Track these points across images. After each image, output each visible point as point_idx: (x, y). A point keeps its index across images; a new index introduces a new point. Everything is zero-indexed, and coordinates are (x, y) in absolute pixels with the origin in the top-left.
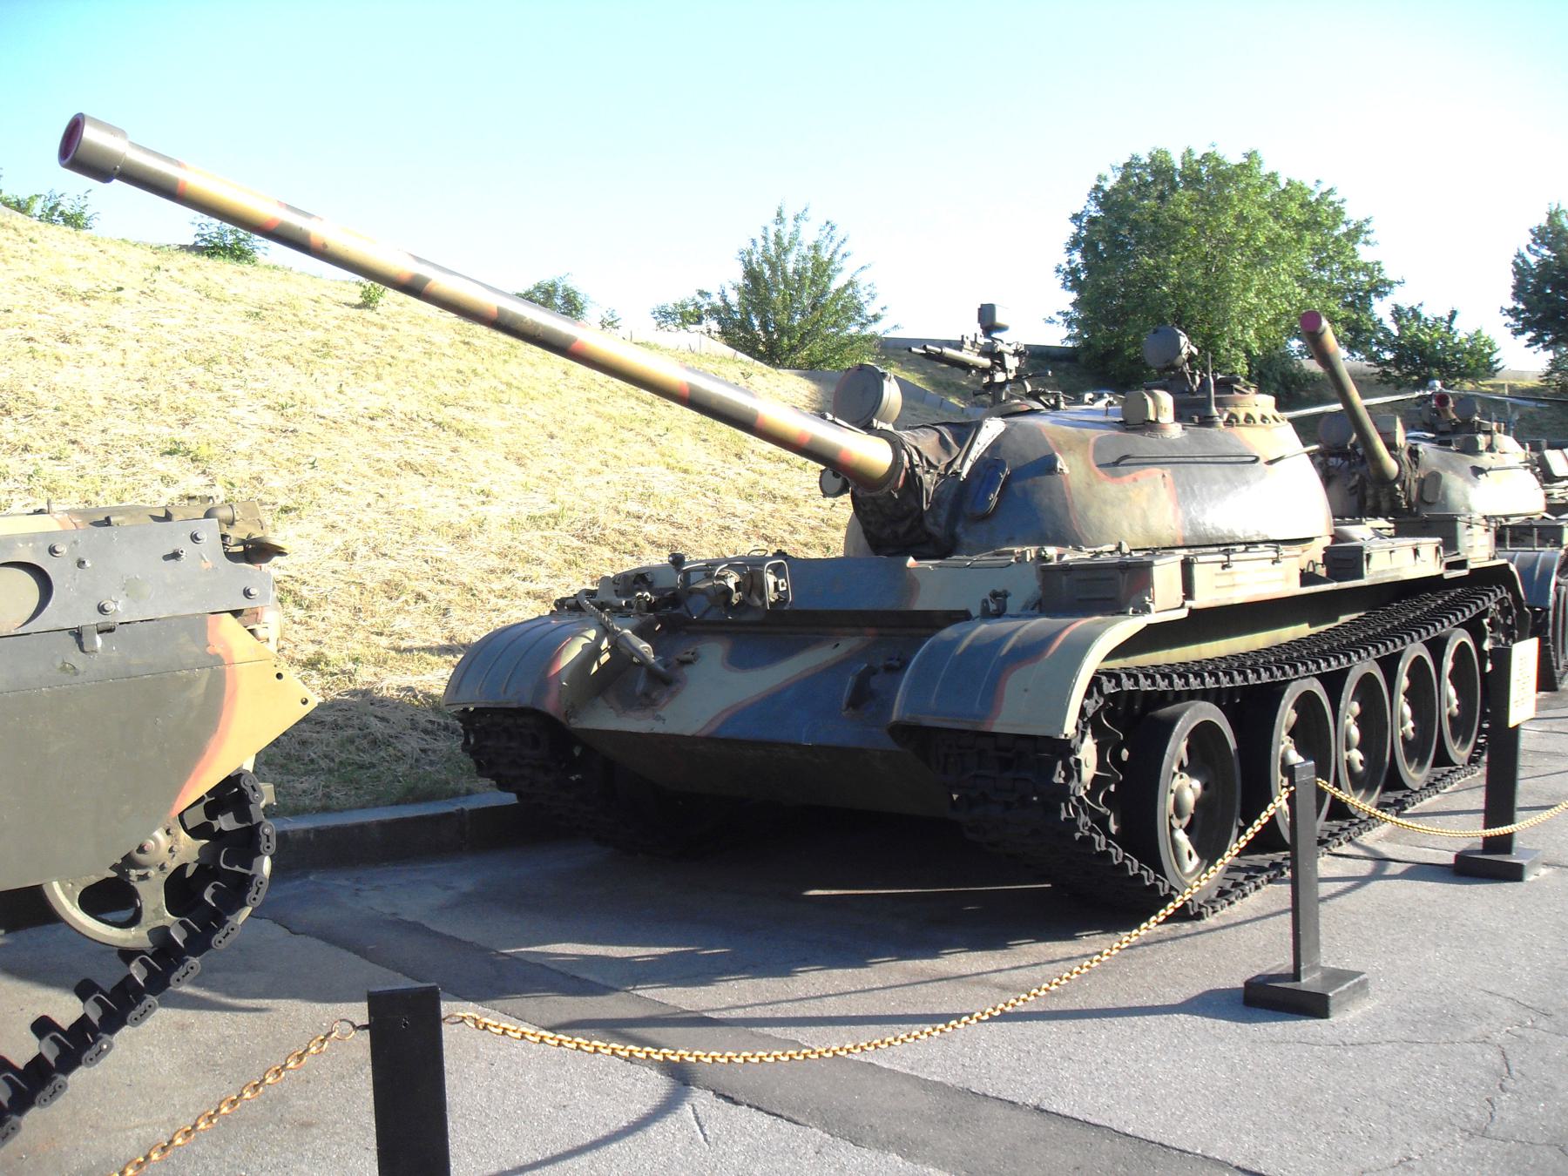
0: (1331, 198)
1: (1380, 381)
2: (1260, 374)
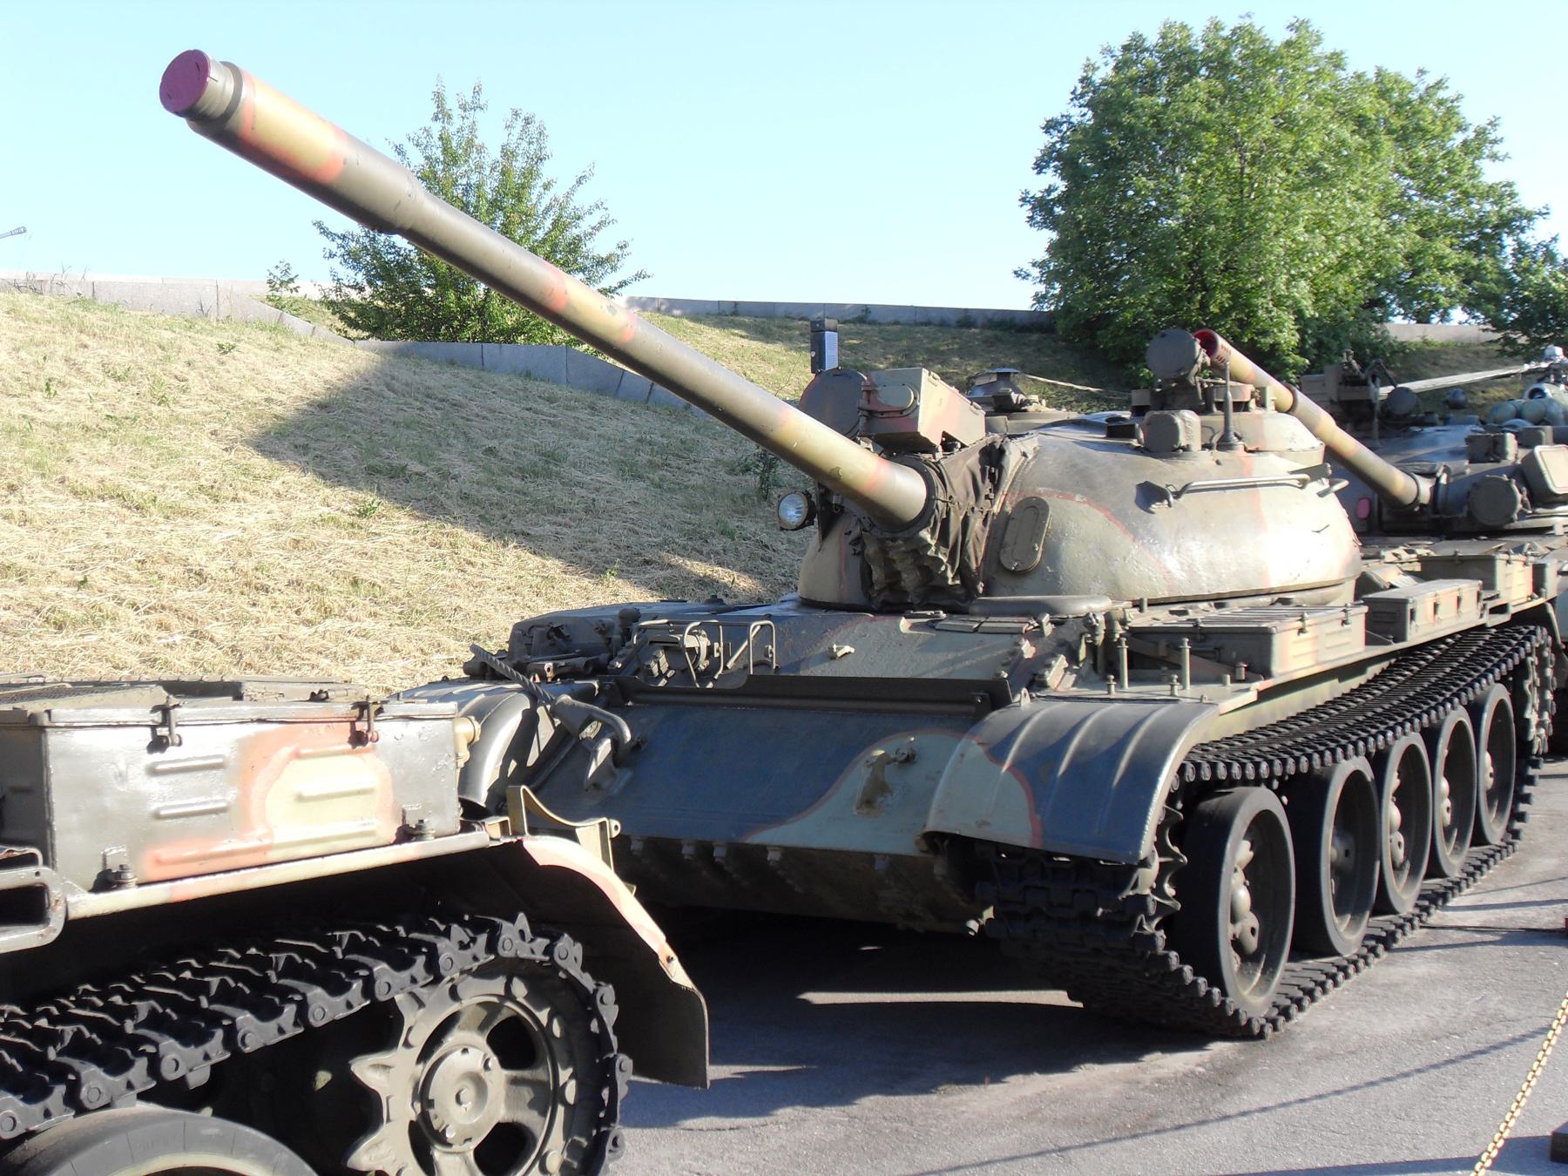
0: (1442, 94)
1: (1502, 352)
2: (1319, 345)
